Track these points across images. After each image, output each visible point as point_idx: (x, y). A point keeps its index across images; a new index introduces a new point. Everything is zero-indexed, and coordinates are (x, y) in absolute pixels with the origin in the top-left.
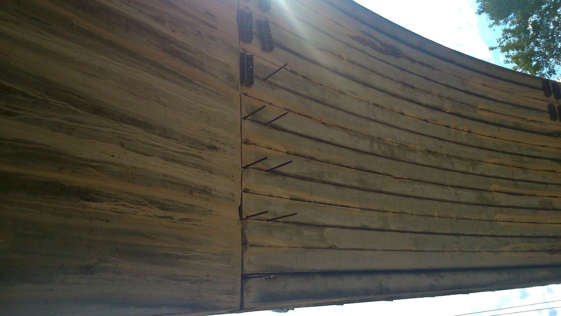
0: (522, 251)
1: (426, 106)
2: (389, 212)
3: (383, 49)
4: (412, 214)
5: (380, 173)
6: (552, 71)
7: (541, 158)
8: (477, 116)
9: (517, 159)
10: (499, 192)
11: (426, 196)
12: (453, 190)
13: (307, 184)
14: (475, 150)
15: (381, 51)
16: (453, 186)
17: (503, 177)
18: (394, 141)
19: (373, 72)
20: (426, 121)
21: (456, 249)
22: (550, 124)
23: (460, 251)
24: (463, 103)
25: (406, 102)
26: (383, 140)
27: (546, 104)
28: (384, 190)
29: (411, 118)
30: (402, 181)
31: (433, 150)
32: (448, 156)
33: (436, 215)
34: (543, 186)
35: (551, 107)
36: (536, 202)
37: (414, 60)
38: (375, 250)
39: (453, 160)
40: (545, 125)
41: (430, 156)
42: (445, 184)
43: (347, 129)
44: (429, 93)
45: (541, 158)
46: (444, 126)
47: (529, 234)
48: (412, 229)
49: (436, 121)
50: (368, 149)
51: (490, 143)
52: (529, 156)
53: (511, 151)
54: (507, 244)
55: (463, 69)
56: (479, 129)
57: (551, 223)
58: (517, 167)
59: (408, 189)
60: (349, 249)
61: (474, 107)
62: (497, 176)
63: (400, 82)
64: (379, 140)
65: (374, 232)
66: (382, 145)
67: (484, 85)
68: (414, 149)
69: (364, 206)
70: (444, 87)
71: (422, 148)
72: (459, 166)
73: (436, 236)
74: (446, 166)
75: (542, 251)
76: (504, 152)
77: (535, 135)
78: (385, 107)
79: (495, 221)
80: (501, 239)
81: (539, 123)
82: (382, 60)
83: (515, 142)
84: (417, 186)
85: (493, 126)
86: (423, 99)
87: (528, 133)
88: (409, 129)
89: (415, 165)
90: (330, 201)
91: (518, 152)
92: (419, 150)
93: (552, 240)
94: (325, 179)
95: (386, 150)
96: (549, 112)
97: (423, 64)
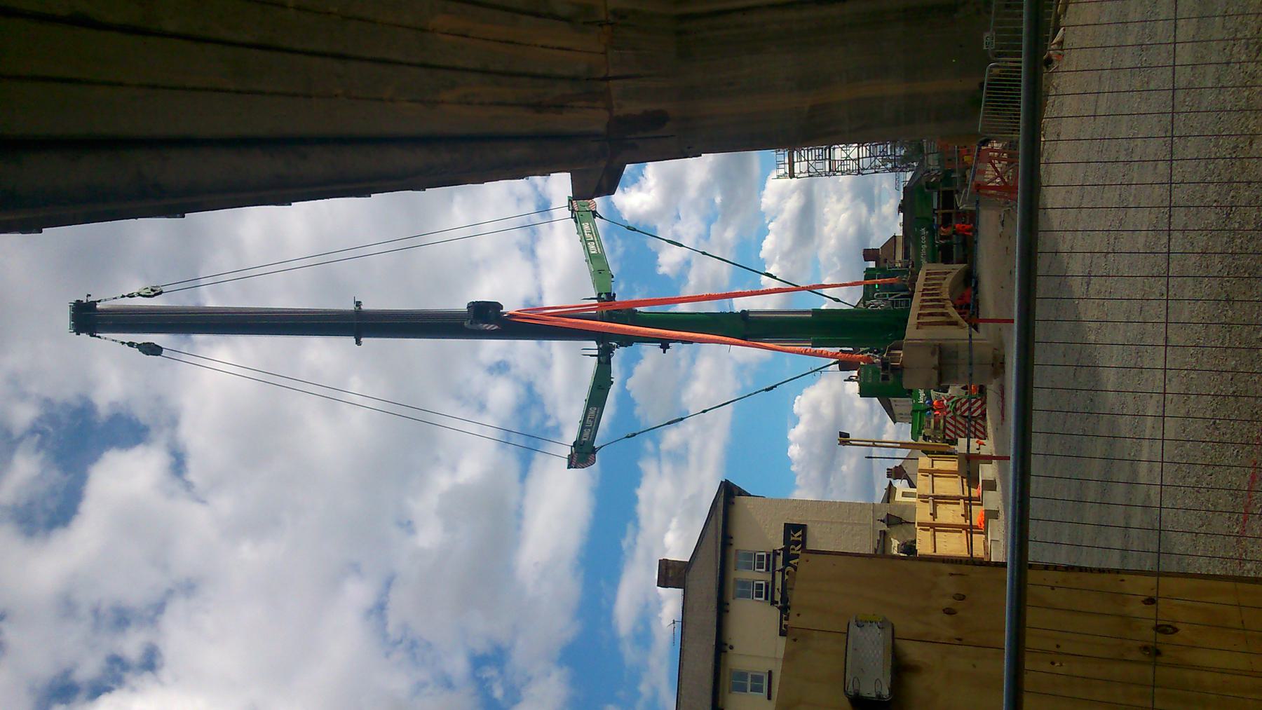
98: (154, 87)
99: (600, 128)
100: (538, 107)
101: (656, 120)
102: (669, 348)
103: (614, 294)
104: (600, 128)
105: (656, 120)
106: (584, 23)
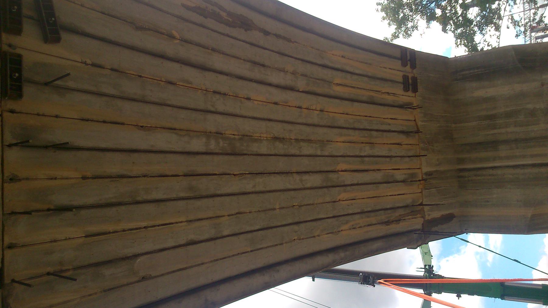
0: (361, 227)
1: (277, 86)
2: (224, 216)
3: (229, 21)
4: (250, 212)
5: (216, 174)
6: (415, 27)
7: (389, 131)
8: (331, 93)
9: (366, 135)
10: (345, 171)
11: (268, 189)
12: (297, 177)
13: (113, 211)
14: (325, 130)
15: (228, 24)
16: (298, 173)
17: (351, 155)
18: (236, 133)
19: (214, 51)
20: (276, 103)
21: (296, 238)
22: (403, 95)
23: (300, 239)
24: (318, 79)
25: (255, 85)
26: (222, 134)
27: (401, 74)
28: (219, 192)
29: (259, 103)
30: (243, 177)
31: (281, 136)
32: (297, 140)
33: (277, 206)
34: (388, 159)
35: (405, 78)
36: (378, 176)
37: (268, 32)
38: (203, 264)
39: (302, 144)
40: (397, 97)
41: (277, 143)
42: (290, 172)
43: (175, 129)
44: (282, 70)
45: (389, 131)
46: (295, 107)
47: (369, 209)
48: (248, 229)
49: (286, 103)
50: (202, 149)
51: (341, 120)
52: (377, 131)
53: (362, 127)
54: (347, 222)
55: (322, 39)
56: (333, 106)
57: (390, 196)
58: (366, 143)
59: (248, 185)
60: (168, 273)
61: (329, 83)
62: (345, 155)
63: (248, 61)
64: (219, 134)
65: (204, 243)
66: (221, 141)
67: (342, 57)
68: (260, 138)
69: (191, 217)
70: (300, 62)
71: (268, 136)
72: (307, 149)
73: (275, 229)
74: (293, 151)
75: (379, 224)
76: (354, 129)
77: (387, 108)
78: (228, 94)
79: (338, 201)
80: (342, 219)
81: (393, 95)
82: (228, 36)
83: (366, 116)
84: (259, 179)
85: (347, 102)
86: (275, 78)
87: (380, 107)
88: (255, 115)
89: (259, 157)
90: (147, 223)
91: (368, 128)
92: (265, 139)
93: (389, 211)
94: (139, 199)
95: (226, 145)
96: (403, 83)
97: (278, 36)
98: (217, 260)
99: (419, 227)
100: (387, 223)
101: (449, 218)
102: (461, 297)
103: (433, 266)
104: (419, 227)
105: (449, 218)
106: (411, 181)
